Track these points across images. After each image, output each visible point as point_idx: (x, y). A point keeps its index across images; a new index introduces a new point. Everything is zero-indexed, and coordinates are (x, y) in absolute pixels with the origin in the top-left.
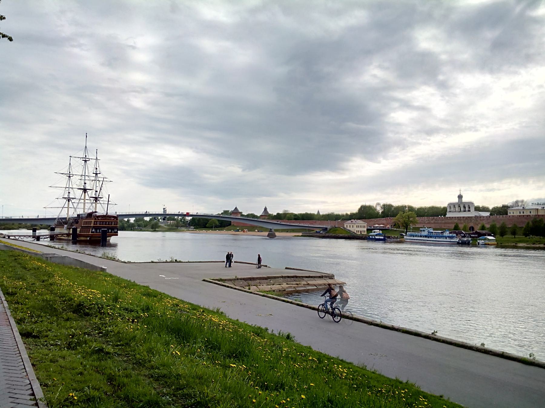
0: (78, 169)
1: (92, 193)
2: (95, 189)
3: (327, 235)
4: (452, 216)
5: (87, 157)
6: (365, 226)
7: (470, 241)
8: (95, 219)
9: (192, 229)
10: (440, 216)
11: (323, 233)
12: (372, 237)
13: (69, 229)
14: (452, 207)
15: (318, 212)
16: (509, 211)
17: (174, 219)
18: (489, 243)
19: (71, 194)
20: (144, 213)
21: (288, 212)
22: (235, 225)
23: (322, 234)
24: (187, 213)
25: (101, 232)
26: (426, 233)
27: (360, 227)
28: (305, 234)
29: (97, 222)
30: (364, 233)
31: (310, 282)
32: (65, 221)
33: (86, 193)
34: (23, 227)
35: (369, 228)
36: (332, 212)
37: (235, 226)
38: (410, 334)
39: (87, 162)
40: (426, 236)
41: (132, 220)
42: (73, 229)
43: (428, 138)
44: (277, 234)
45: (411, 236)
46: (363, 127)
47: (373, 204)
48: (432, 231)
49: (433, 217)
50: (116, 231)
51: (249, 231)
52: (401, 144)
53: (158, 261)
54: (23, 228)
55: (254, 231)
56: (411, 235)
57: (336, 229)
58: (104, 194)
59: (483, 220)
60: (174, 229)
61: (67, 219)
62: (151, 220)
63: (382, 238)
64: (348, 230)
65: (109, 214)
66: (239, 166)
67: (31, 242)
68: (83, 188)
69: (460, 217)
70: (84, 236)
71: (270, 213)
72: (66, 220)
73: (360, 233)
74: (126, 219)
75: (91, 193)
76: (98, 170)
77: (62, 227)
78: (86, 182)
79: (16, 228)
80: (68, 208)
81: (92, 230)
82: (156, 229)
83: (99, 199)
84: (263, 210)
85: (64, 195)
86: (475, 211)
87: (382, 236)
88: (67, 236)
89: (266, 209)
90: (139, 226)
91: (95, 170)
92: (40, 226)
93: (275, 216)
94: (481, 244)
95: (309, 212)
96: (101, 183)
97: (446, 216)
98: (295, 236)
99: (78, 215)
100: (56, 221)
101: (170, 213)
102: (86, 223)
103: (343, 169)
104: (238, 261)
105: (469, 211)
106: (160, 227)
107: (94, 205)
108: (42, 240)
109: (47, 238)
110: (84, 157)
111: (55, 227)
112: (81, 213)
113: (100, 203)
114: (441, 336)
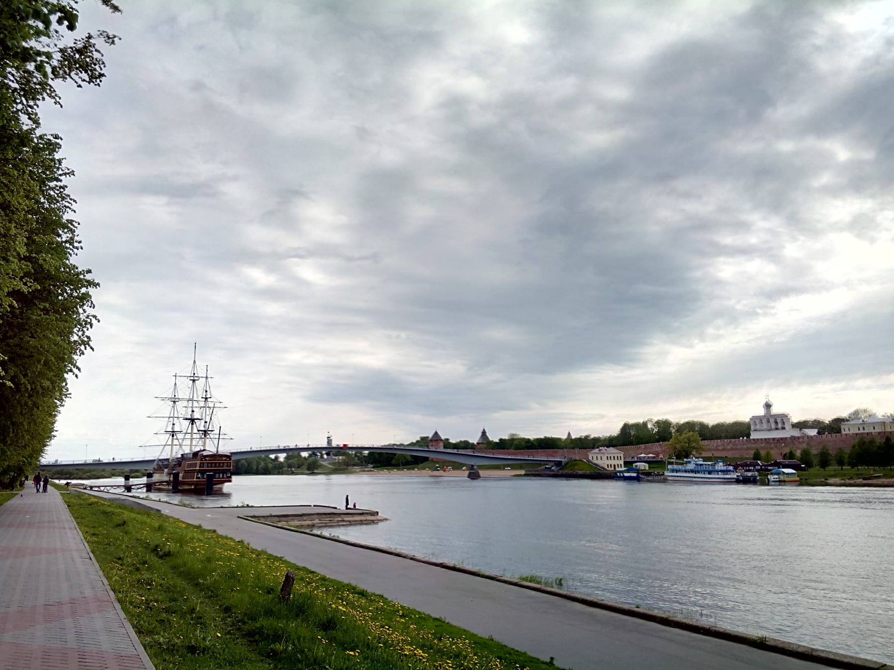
3: (560, 472)
4: (765, 437)
5: (196, 375)
6: (620, 457)
7: (756, 477)
8: (202, 460)
10: (741, 438)
12: (219, 476)
14: (757, 422)
16: (842, 427)
18: (786, 479)
19: (175, 426)
23: (553, 471)
25: (205, 476)
26: (691, 466)
27: (612, 458)
29: (203, 463)
31: (345, 519)
32: (168, 463)
33: (194, 425)
34: (117, 474)
35: (627, 460)
38: (449, 570)
39: (196, 381)
40: (692, 471)
41: (282, 457)
43: (772, 304)
44: (482, 473)
45: (673, 471)
48: (702, 463)
49: (729, 440)
53: (228, 506)
58: (215, 426)
59: (803, 442)
60: (341, 470)
61: (170, 461)
62: (310, 456)
63: (635, 475)
64: (595, 464)
67: (122, 493)
69: (769, 439)
71: (491, 439)
73: (613, 469)
74: (273, 456)
75: (200, 425)
76: (208, 393)
77: (162, 471)
78: (194, 410)
81: (197, 475)
82: (313, 470)
83: (209, 432)
84: (480, 434)
85: (166, 429)
86: (792, 428)
87: (635, 473)
88: (166, 485)
89: (484, 433)
90: (290, 466)
91: (204, 393)
93: (496, 443)
94: (773, 481)
96: (212, 409)
97: (751, 438)
100: (156, 462)
102: (189, 466)
105: (783, 428)
106: (321, 466)
108: (134, 491)
109: (141, 488)
110: (192, 375)
111: (153, 473)
112: (186, 452)
113: (211, 438)
114: (869, 657)
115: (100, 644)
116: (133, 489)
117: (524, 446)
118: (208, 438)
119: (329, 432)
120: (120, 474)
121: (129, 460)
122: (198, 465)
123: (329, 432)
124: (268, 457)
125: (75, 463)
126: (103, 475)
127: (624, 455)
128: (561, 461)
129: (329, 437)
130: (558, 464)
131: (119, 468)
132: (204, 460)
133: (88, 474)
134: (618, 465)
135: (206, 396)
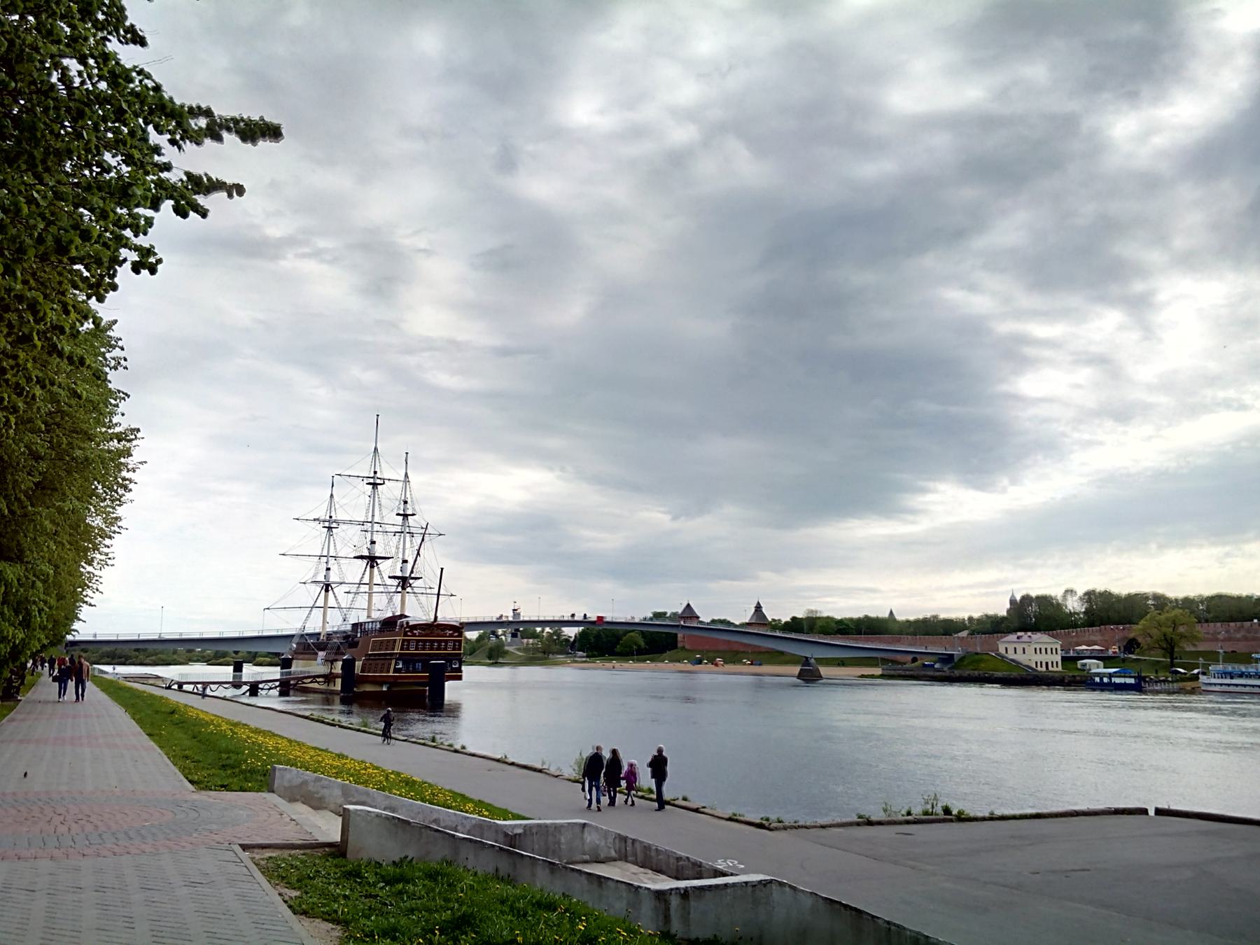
0: (353, 503)
1: (394, 566)
2: (401, 556)
5: (378, 475)
6: (1056, 649)
9: (584, 659)
11: (946, 669)
12: (1101, 679)
13: (332, 662)
15: (891, 612)
17: (534, 636)
19: (331, 572)
20: (495, 620)
21: (818, 615)
22: (687, 647)
23: (938, 670)
24: (598, 617)
27: (1043, 651)
28: (892, 673)
29: (409, 641)
30: (1055, 669)
32: (316, 641)
36: (934, 614)
37: (686, 650)
39: (379, 486)
42: (344, 661)
44: (824, 671)
45: (1225, 674)
46: (954, 410)
47: (1056, 592)
50: (457, 666)
51: (726, 662)
52: (1050, 447)
54: (195, 661)
55: (739, 662)
56: (1225, 673)
57: (976, 657)
60: (539, 659)
62: (480, 638)
63: (1132, 681)
64: (1013, 660)
65: (441, 620)
66: (662, 509)
68: (368, 554)
70: (374, 681)
72: (318, 639)
73: (1044, 669)
79: (182, 660)
80: (325, 607)
81: (396, 665)
83: (411, 581)
84: (753, 610)
87: (1131, 677)
88: (325, 682)
89: (758, 608)
91: (402, 506)
92: (234, 655)
95: (873, 615)
96: (418, 539)
98: (863, 676)
99: (355, 626)
100: (296, 640)
101: (526, 619)
103: (913, 512)
104: (1173, 807)
106: (507, 652)
107: (398, 597)
108: (264, 692)
110: (372, 475)
111: (292, 659)
115: (188, 932)
116: (262, 689)
117: (836, 629)
118: (408, 593)
119: (515, 602)
120: (199, 658)
121: (255, 634)
122: (399, 645)
123: (515, 602)
124: (558, 634)
125: (141, 638)
126: (175, 660)
127: (1061, 646)
128: (953, 655)
129: (516, 610)
130: (947, 659)
131: (230, 649)
132: (409, 634)
133: (154, 658)
134: (1052, 663)
135: (404, 511)
